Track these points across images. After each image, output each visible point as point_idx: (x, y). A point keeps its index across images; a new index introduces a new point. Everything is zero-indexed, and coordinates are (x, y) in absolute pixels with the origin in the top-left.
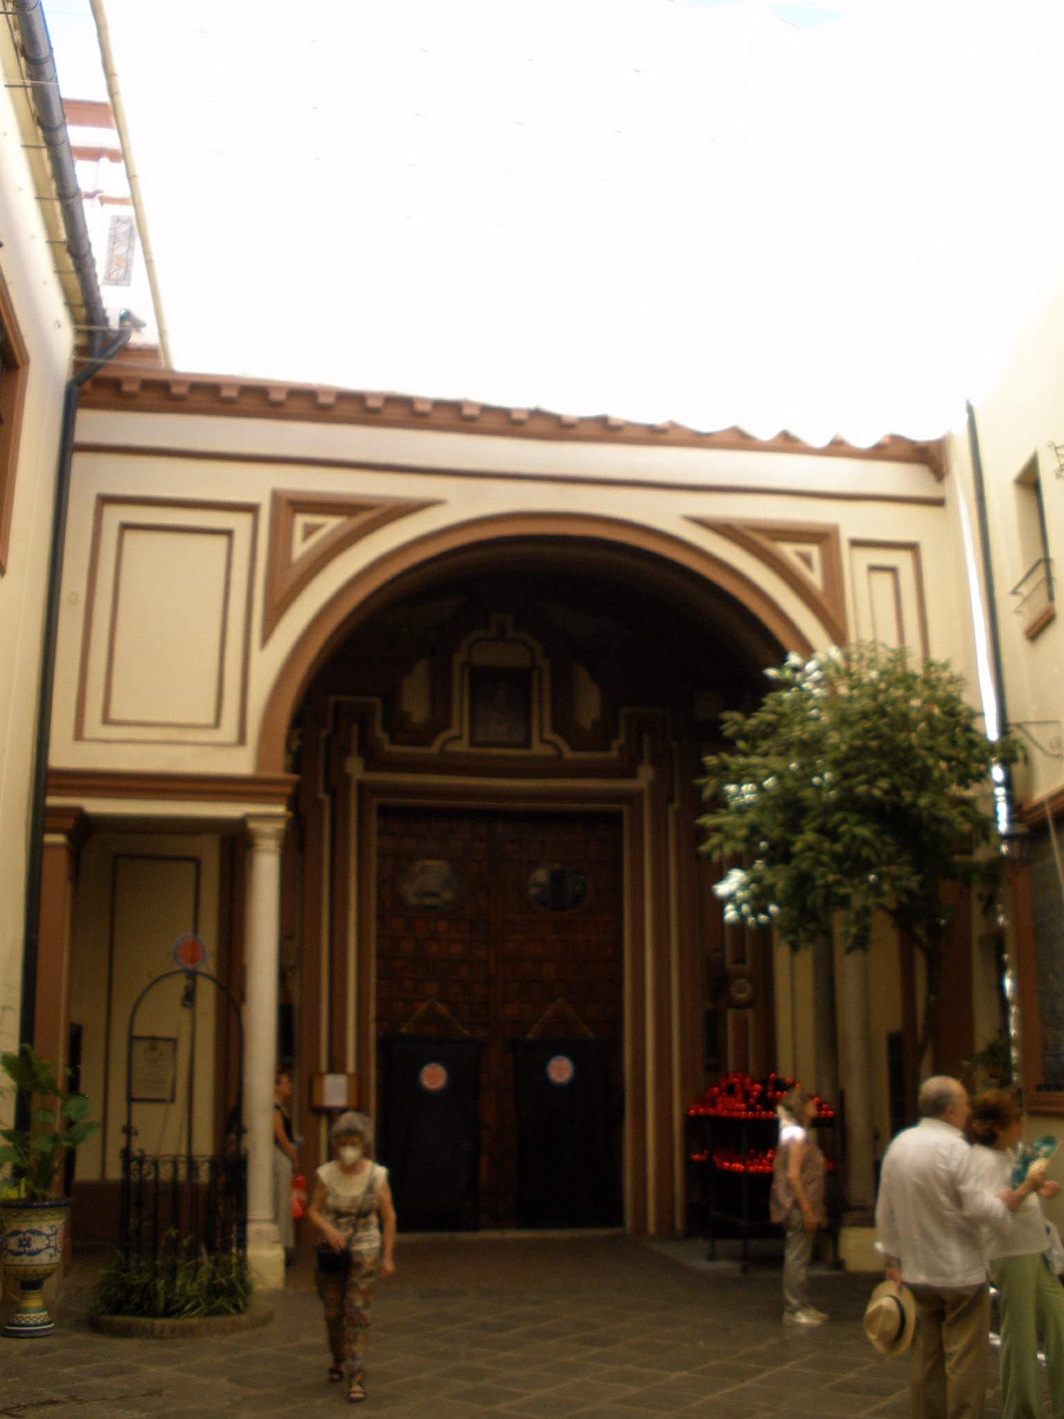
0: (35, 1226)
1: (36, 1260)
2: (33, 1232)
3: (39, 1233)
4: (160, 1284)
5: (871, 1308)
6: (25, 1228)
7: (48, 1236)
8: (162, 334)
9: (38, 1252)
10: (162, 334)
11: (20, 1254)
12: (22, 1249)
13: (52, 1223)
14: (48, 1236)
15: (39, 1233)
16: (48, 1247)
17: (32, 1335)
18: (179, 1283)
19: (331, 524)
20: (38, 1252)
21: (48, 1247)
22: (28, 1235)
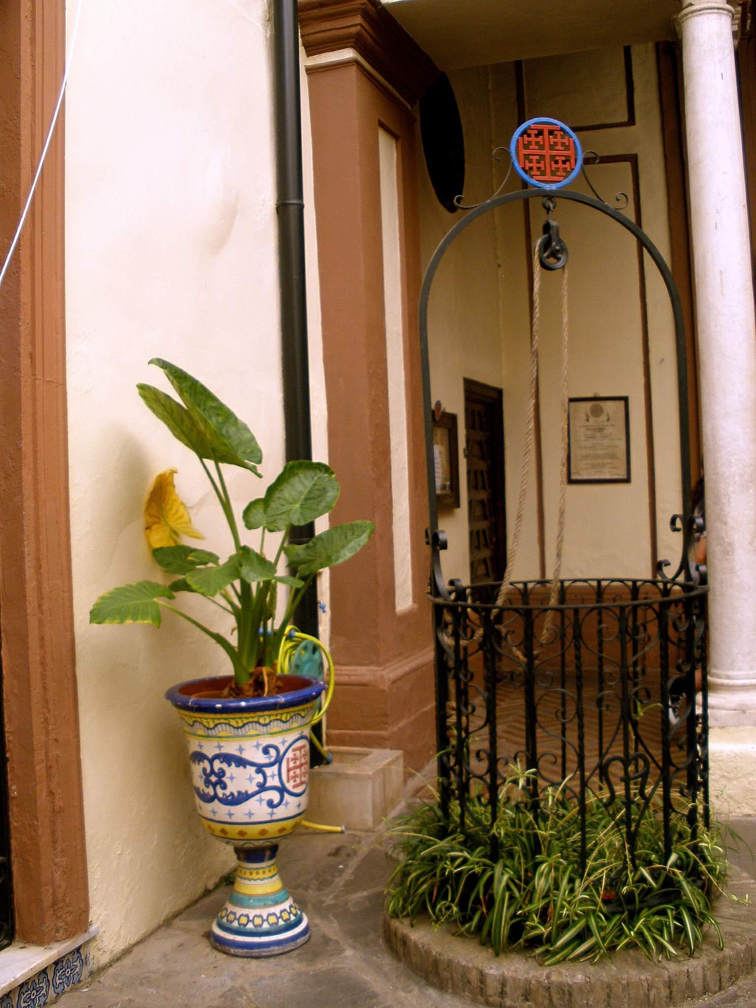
0: (230, 748)
1: (239, 812)
2: (228, 759)
3: (241, 762)
4: (502, 877)
5: (352, 554)
6: (210, 750)
7: (260, 768)
8: (594, 580)
9: (242, 798)
10: (594, 580)
11: (210, 799)
12: (210, 791)
13: (265, 741)
14: (260, 768)
15: (241, 762)
16: (262, 788)
17: (251, 952)
18: (541, 884)
19: (632, 218)
20: (242, 798)
21: (262, 788)
22: (217, 765)
